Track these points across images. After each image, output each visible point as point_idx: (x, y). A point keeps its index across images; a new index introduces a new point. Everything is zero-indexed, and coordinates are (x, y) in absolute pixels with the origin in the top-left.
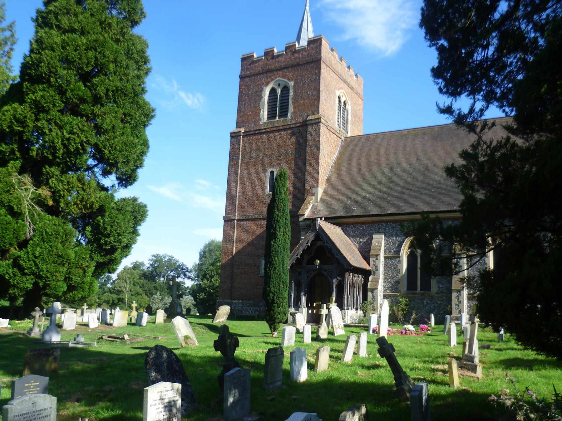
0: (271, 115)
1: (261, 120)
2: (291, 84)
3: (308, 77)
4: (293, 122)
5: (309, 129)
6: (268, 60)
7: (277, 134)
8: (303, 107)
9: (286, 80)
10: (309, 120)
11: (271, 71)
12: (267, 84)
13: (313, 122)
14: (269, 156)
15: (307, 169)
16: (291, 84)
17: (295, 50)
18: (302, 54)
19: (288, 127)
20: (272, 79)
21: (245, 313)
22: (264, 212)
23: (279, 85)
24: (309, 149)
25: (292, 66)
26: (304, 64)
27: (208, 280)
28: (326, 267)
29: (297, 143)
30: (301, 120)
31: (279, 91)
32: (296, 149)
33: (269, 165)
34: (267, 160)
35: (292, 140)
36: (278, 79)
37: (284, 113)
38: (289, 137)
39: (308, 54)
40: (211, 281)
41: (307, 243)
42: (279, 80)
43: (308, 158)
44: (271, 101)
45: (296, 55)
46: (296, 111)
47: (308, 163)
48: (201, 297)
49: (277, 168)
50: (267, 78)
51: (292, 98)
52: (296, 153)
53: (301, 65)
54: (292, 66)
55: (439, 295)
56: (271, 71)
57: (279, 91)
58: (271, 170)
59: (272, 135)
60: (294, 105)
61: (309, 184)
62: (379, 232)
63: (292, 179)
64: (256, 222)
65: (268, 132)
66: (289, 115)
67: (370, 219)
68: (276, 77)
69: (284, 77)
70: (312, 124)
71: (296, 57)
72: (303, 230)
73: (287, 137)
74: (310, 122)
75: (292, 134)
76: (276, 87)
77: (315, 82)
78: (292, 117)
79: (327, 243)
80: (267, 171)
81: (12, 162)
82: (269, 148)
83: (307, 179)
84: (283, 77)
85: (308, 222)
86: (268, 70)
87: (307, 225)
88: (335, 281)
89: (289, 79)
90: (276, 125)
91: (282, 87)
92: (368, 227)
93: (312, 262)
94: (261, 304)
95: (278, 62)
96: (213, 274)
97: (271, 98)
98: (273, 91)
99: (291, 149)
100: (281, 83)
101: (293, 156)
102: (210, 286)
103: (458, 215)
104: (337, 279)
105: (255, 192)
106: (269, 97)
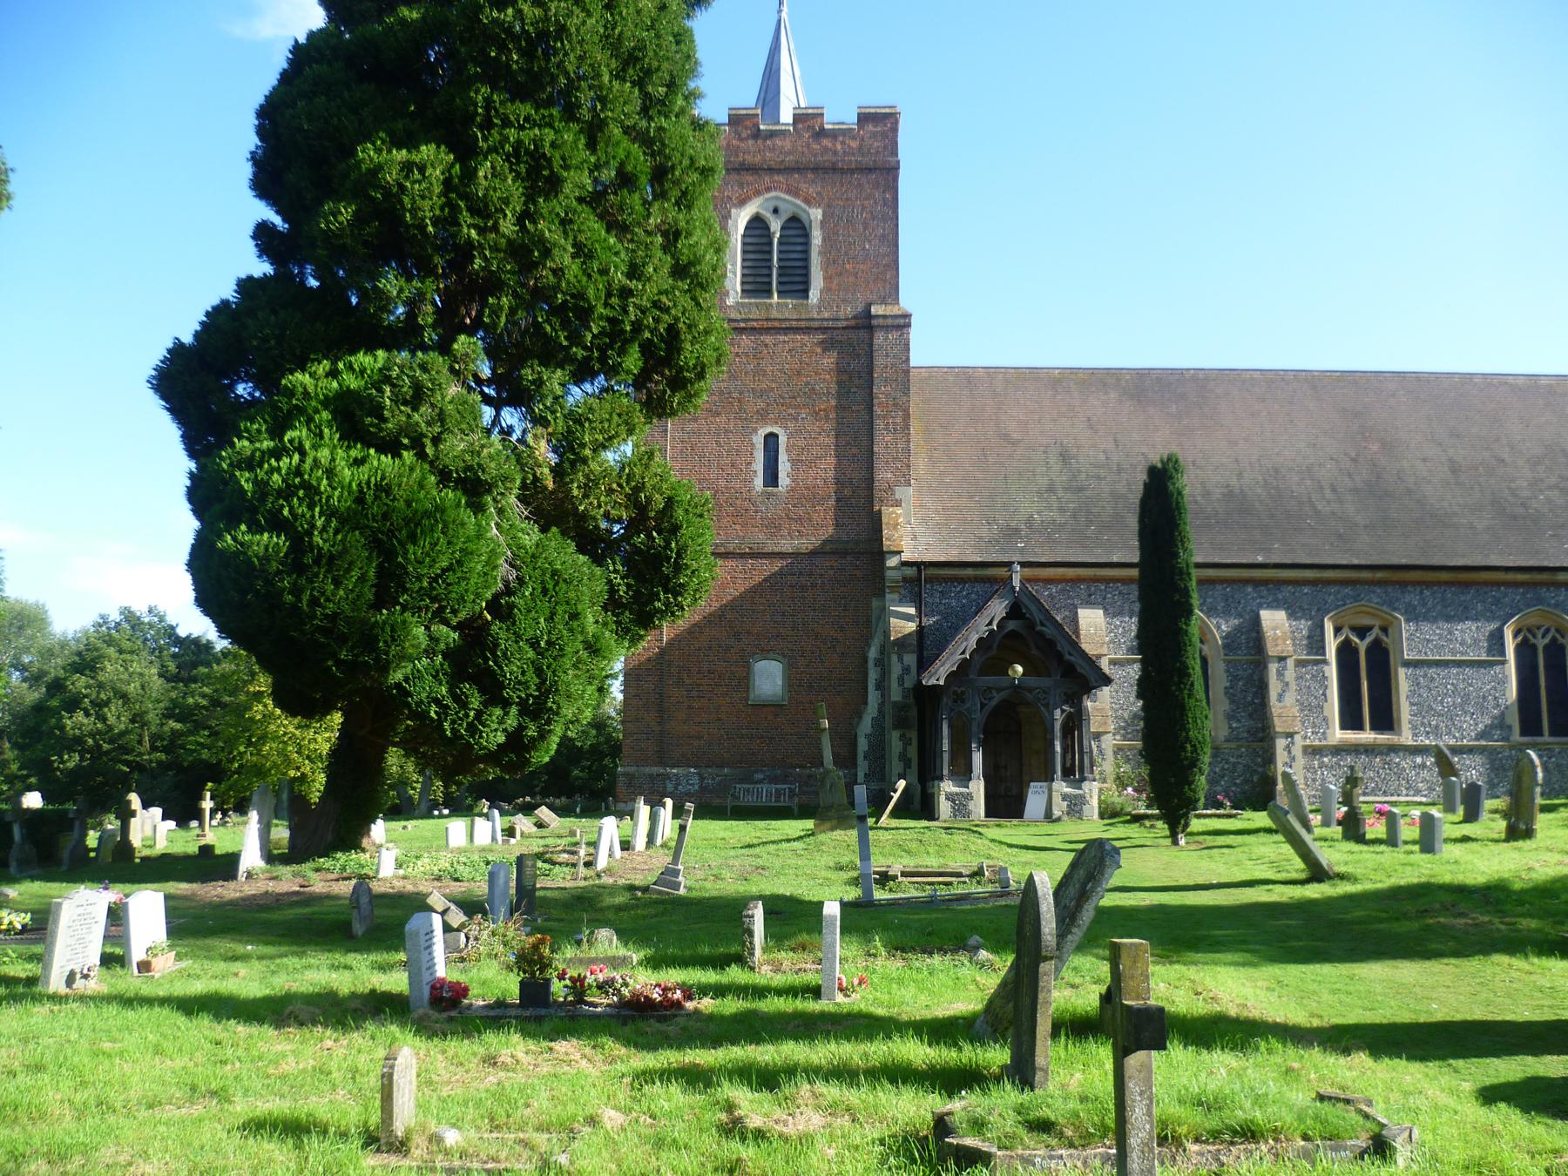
0: (756, 285)
1: (727, 294)
2: (816, 214)
3: (864, 208)
4: (826, 315)
5: (879, 337)
6: (741, 139)
7: (782, 338)
8: (852, 279)
9: (798, 202)
10: (877, 316)
11: (754, 169)
12: (742, 202)
13: (890, 321)
14: (762, 394)
15: (877, 439)
16: (816, 214)
17: (822, 129)
18: (843, 143)
19: (816, 324)
20: (758, 193)
21: (748, 800)
22: (1128, 550)
23: (776, 211)
24: (881, 391)
25: (816, 169)
26: (852, 171)
27: (87, 714)
28: (1033, 681)
29: (840, 370)
30: (849, 311)
31: (776, 226)
32: (839, 383)
33: (763, 416)
34: (754, 405)
35: (829, 360)
36: (773, 194)
37: (797, 284)
38: (819, 350)
39: (860, 147)
40: (104, 719)
41: (990, 623)
42: (777, 198)
43: (878, 410)
44: (750, 248)
45: (826, 142)
46: (834, 286)
47: (879, 424)
48: (71, 765)
49: (786, 428)
50: (741, 185)
51: (820, 253)
52: (839, 395)
53: (843, 171)
54: (816, 169)
55: (1233, 745)
56: (754, 169)
57: (776, 226)
58: (769, 429)
59: (768, 339)
60: (825, 269)
61: (883, 475)
62: (1089, 603)
63: (833, 460)
64: (731, 563)
65: (753, 329)
66: (814, 295)
67: (1308, 574)
68: (768, 189)
69: (794, 192)
70: (887, 328)
71: (826, 149)
72: (893, 590)
73: (812, 352)
74: (881, 321)
75: (827, 346)
76: (768, 215)
77: (885, 221)
78: (821, 300)
79: (1042, 624)
80: (755, 430)
81: (462, 338)
82: (759, 372)
83: (879, 464)
84: (789, 192)
85: (911, 572)
86: (742, 164)
87: (905, 579)
88: (1057, 713)
89: (807, 201)
90: (774, 314)
91: (785, 217)
92: (1063, 590)
93: (1002, 669)
94: (759, 776)
95: (772, 150)
96: (103, 696)
97: (749, 240)
98: (757, 223)
99: (826, 383)
100: (782, 206)
101: (833, 402)
102: (99, 732)
103: (1135, 572)
104: (1063, 711)
105: (722, 483)
106: (744, 236)
